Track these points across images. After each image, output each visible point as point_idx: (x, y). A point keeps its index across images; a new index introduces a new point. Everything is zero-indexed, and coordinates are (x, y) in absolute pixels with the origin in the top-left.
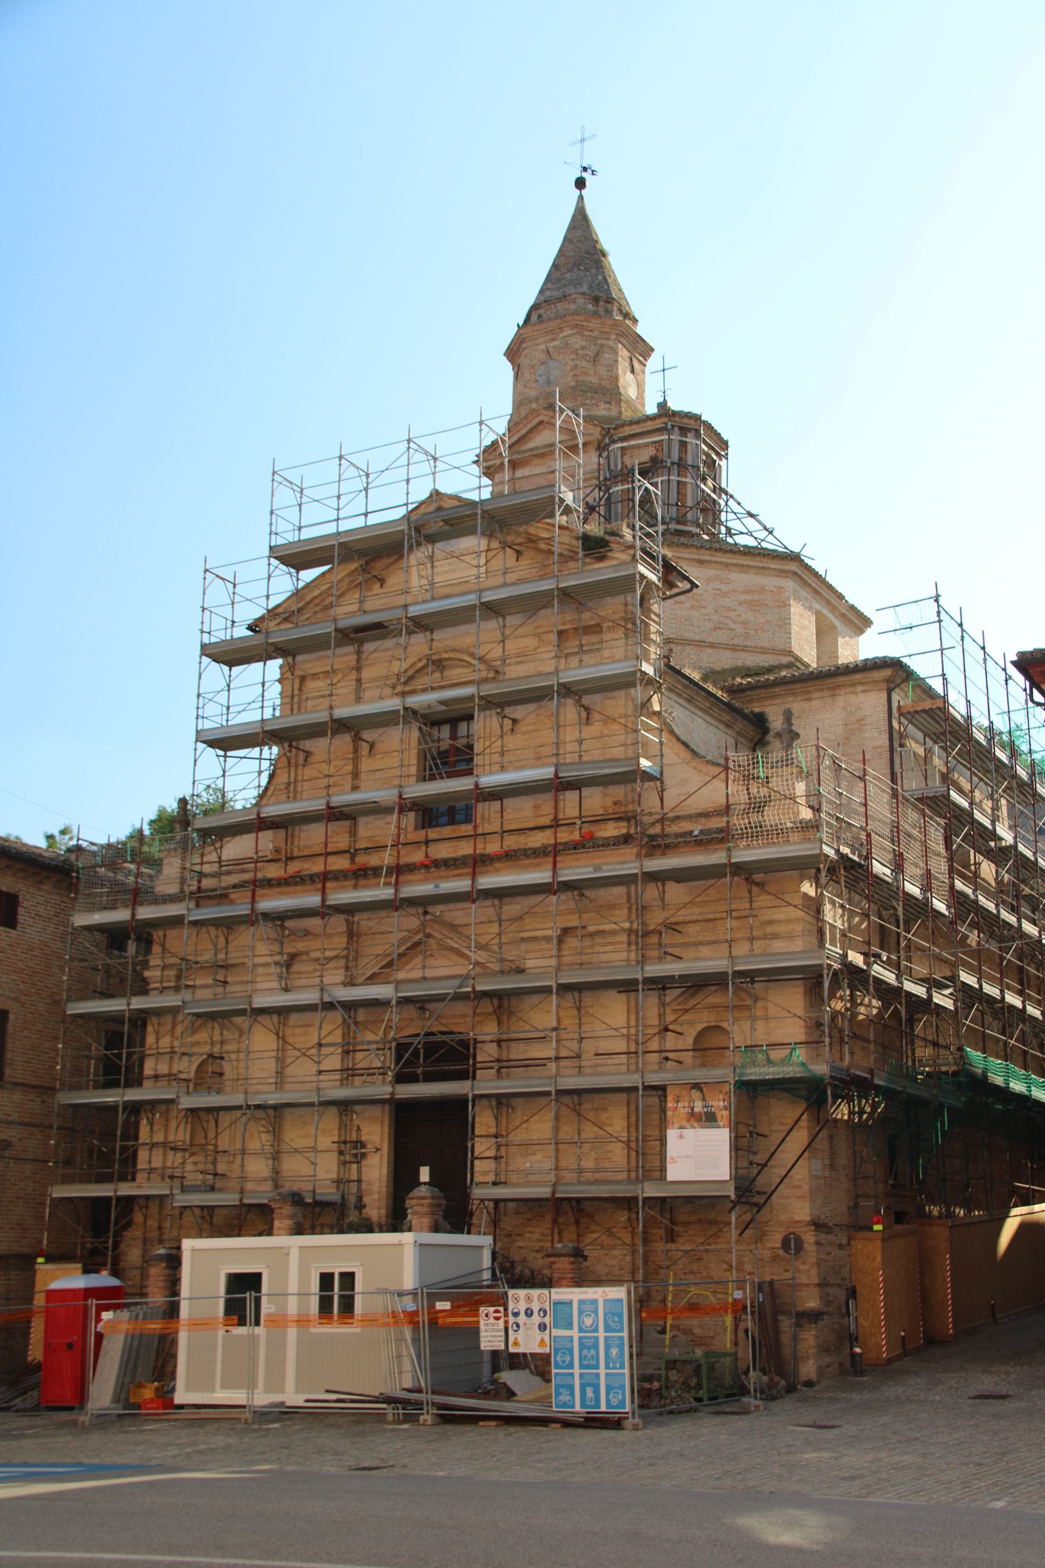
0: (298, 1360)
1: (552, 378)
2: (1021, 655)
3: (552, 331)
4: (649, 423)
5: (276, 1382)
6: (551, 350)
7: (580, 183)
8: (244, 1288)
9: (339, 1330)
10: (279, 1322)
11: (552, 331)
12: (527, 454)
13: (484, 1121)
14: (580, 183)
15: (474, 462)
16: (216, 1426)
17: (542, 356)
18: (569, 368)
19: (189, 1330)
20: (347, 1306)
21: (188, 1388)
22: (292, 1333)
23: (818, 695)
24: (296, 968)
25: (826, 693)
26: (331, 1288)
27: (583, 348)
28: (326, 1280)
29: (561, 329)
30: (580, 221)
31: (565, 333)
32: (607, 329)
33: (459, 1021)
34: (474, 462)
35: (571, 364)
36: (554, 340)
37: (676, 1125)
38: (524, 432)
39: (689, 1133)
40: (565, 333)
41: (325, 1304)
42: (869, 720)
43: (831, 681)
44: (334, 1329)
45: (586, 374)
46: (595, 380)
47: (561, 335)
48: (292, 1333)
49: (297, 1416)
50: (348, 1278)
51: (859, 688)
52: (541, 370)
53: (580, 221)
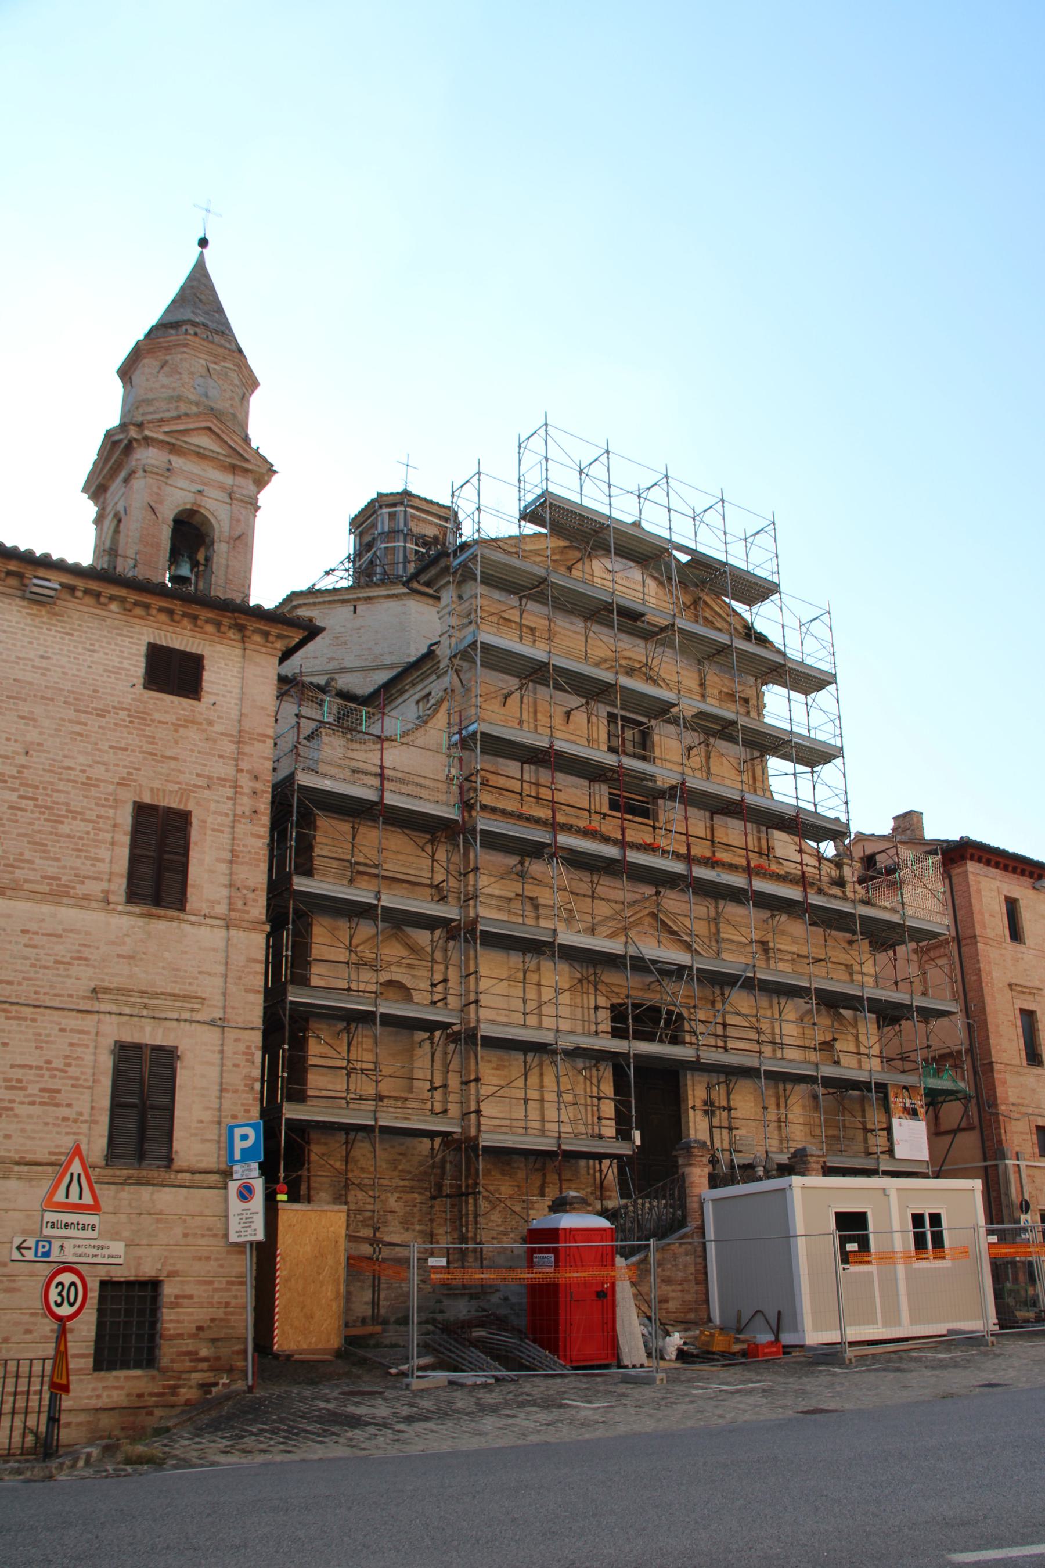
0: (909, 1294)
3: (216, 356)
4: (436, 507)
5: (892, 1317)
7: (203, 243)
8: (852, 1224)
9: (933, 1266)
10: (888, 1258)
11: (216, 356)
13: (695, 1092)
14: (203, 243)
19: (905, 1263)
20: (938, 1240)
21: (816, 1328)
22: (900, 1269)
26: (923, 1226)
28: (918, 1220)
29: (225, 359)
31: (226, 365)
33: (675, 996)
36: (215, 363)
37: (897, 1115)
38: (191, 426)
39: (904, 1121)
40: (226, 365)
41: (920, 1241)
44: (929, 1264)
47: (223, 364)
48: (900, 1269)
49: (599, 1379)
50: (936, 1219)
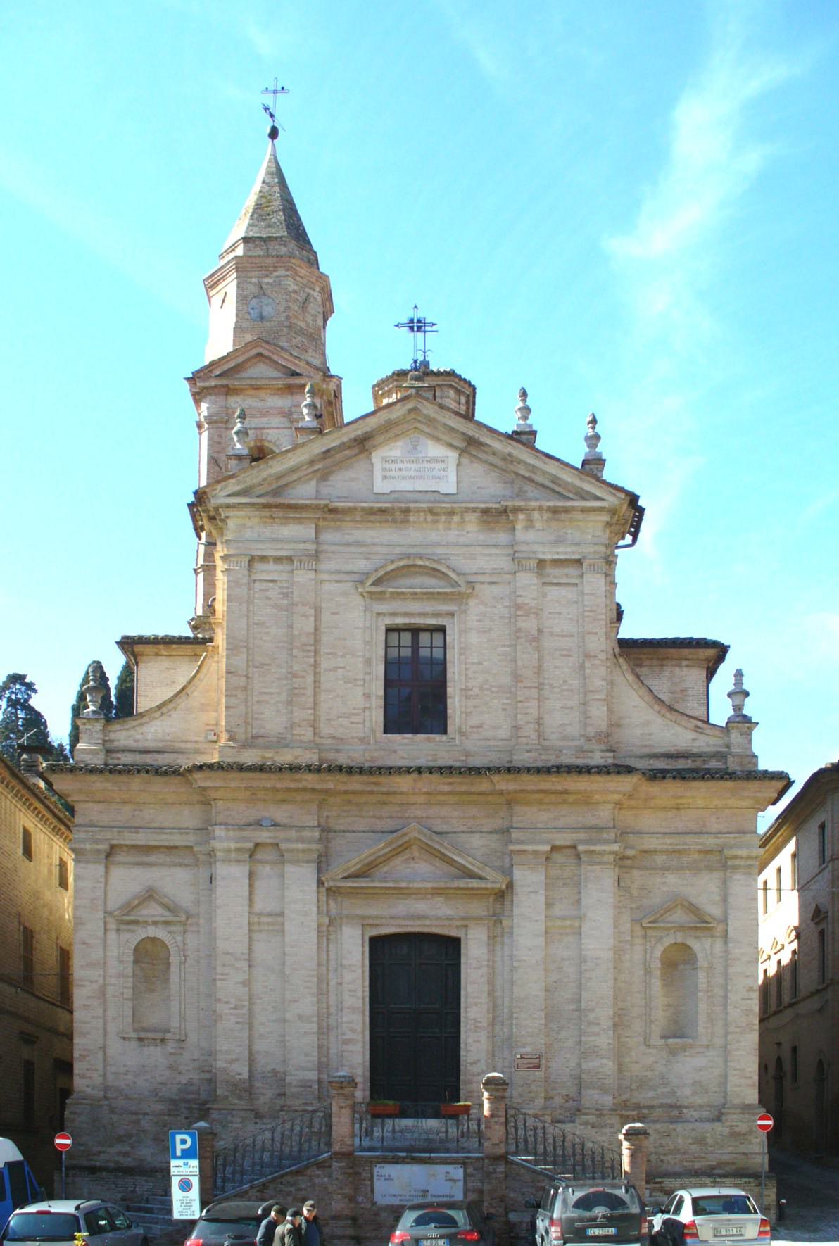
1: (265, 314)
2: (125, 638)
6: (264, 286)
12: (244, 383)
15: (187, 379)
16: (697, 1165)
17: (255, 290)
18: (282, 309)
23: (648, 663)
24: (258, 856)
25: (655, 662)
27: (295, 292)
30: (278, 176)
32: (314, 280)
34: (187, 379)
35: (284, 305)
42: (690, 692)
43: (663, 651)
45: (297, 318)
46: (302, 324)
51: (684, 663)
52: (254, 302)
53: (278, 176)
